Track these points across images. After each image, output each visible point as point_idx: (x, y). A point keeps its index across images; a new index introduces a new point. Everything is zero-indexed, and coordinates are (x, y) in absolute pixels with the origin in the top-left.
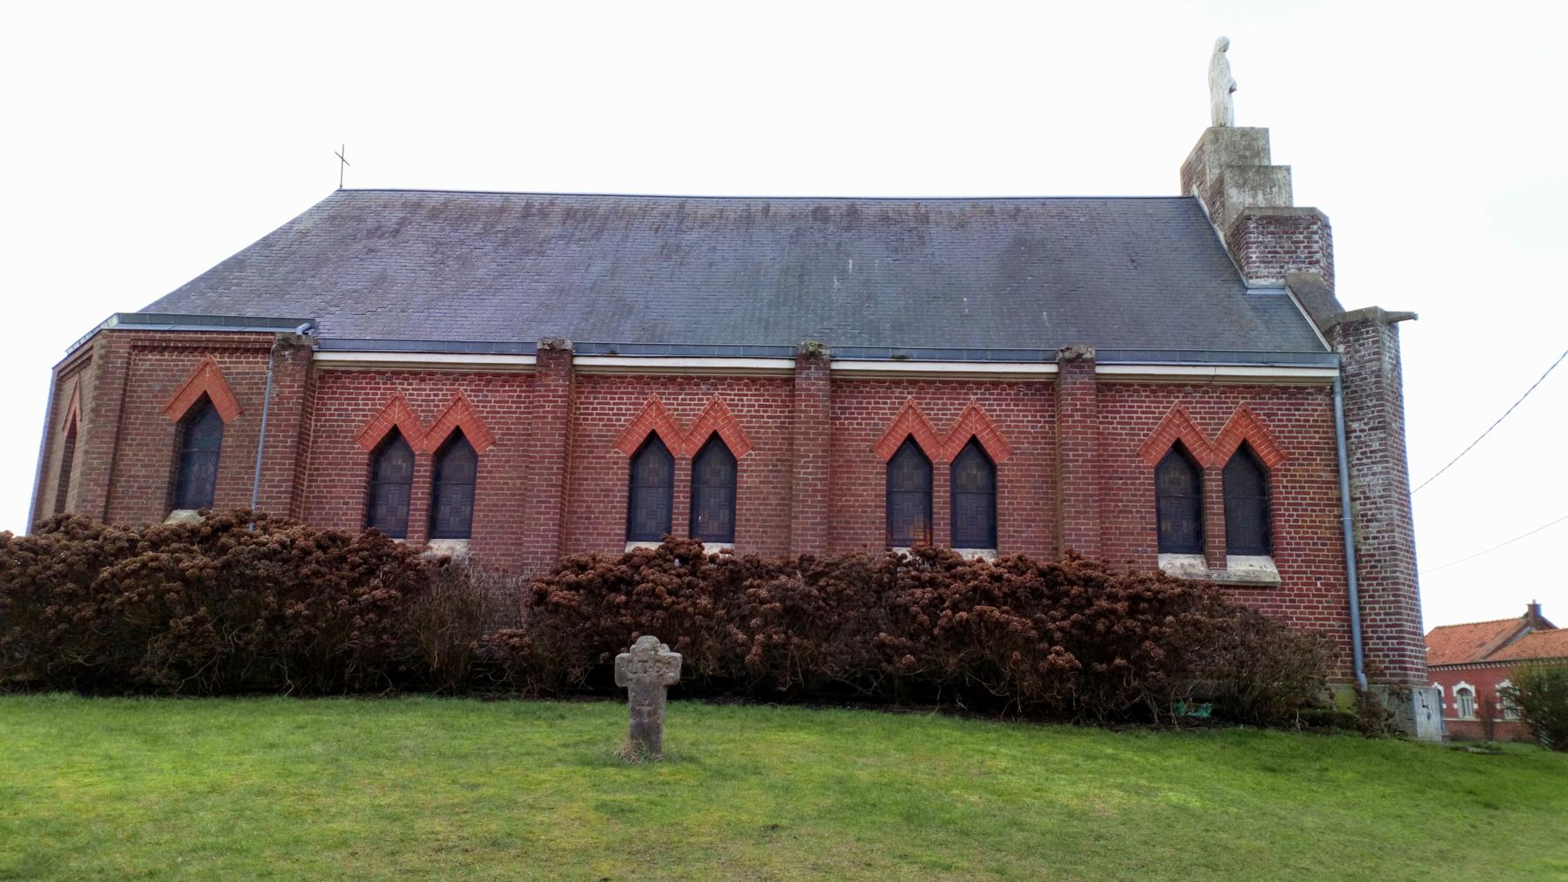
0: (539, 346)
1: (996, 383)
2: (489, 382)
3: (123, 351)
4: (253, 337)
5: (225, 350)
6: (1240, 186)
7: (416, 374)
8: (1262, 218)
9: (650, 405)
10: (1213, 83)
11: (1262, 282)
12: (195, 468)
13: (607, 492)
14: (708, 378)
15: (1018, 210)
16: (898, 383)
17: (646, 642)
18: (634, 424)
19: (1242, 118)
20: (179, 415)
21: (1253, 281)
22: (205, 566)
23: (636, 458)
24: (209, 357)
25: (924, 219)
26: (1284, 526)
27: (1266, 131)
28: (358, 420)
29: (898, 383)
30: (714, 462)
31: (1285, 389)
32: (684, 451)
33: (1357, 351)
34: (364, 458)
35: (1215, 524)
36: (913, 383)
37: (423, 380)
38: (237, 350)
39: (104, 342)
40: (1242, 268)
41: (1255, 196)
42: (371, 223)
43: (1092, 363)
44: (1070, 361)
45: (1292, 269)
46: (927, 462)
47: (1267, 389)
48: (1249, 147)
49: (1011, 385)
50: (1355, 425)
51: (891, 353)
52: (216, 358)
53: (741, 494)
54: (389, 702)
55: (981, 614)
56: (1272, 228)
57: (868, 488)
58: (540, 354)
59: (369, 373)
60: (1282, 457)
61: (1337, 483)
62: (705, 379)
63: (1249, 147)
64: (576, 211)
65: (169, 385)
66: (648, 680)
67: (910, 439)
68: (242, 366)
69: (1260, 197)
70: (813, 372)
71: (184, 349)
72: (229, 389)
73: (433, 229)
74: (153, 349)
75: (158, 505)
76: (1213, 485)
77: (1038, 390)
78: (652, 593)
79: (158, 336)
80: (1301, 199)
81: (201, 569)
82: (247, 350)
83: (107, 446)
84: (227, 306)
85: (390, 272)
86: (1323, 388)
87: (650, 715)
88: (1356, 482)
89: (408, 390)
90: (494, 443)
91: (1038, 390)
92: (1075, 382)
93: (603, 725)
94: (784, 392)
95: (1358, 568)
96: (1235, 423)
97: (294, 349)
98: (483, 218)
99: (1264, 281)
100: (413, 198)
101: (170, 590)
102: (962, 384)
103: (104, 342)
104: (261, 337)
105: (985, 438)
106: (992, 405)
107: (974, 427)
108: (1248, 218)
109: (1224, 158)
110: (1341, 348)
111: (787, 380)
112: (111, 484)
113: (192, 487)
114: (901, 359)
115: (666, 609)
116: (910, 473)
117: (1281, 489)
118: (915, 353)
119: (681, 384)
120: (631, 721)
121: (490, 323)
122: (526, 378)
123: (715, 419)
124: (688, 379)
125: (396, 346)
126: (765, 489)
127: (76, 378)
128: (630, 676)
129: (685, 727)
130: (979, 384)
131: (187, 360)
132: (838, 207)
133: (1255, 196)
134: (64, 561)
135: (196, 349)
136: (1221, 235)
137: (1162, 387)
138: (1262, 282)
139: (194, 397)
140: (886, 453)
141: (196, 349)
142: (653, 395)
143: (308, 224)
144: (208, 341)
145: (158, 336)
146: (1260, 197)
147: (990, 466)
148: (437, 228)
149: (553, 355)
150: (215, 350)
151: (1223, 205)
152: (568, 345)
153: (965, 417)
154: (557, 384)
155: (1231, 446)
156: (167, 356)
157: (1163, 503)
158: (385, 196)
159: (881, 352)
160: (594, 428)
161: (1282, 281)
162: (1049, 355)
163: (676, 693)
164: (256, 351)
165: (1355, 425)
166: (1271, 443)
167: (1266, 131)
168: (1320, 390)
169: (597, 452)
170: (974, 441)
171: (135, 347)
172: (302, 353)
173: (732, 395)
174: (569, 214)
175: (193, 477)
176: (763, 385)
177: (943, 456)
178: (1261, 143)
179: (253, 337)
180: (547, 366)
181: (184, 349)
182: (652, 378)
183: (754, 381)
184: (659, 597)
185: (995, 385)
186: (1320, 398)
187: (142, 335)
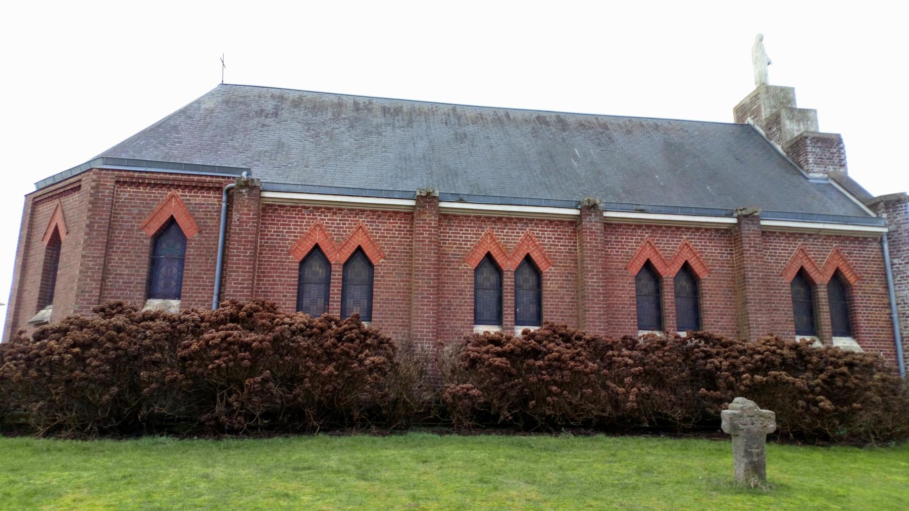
0: (418, 194)
1: (697, 229)
2: (379, 216)
3: (110, 184)
4: (208, 179)
5: (186, 187)
6: (791, 119)
7: (329, 209)
8: (813, 138)
9: (486, 235)
10: (756, 61)
11: (816, 175)
12: (163, 270)
13: (461, 292)
14: (522, 219)
15: (657, 125)
16: (639, 227)
17: (740, 402)
18: (476, 247)
19: (774, 80)
20: (153, 231)
21: (811, 175)
22: (263, 340)
23: (303, 263)
24: (173, 191)
25: (605, 126)
26: (862, 317)
27: (793, 89)
28: (294, 238)
29: (639, 227)
30: (358, 265)
31: (857, 238)
32: (337, 258)
33: (895, 218)
34: (296, 265)
35: (825, 317)
36: (649, 227)
37: (335, 213)
38: (195, 187)
39: (94, 177)
40: (802, 167)
41: (799, 126)
42: (254, 106)
43: (758, 219)
44: (746, 216)
45: (831, 169)
46: (328, 264)
47: (847, 238)
48: (785, 97)
49: (707, 230)
50: (896, 261)
51: (635, 207)
52: (179, 193)
53: (545, 294)
54: (379, 439)
55: (775, 377)
56: (819, 144)
57: (626, 291)
58: (419, 199)
59: (297, 207)
60: (858, 278)
61: (888, 294)
62: (520, 220)
63: (785, 97)
64: (389, 109)
65: (146, 211)
66: (755, 430)
67: (359, 249)
68: (199, 198)
69: (802, 126)
70: (593, 218)
71: (156, 185)
72: (191, 214)
73: (299, 114)
74: (131, 184)
75: (139, 295)
76: (823, 294)
77: (722, 233)
78: (558, 359)
79: (136, 175)
80: (825, 127)
81: (261, 342)
82: (202, 188)
83: (99, 252)
84: (178, 155)
85: (284, 140)
86: (878, 239)
87: (758, 455)
88: (899, 294)
89: (325, 219)
90: (385, 258)
91: (722, 233)
92: (748, 230)
93: (728, 462)
94: (570, 229)
95: (903, 345)
96: (832, 257)
97: (236, 190)
98: (330, 109)
99: (817, 175)
100: (278, 93)
101: (243, 359)
102: (678, 228)
103: (94, 177)
104: (214, 179)
105: (693, 263)
106: (698, 243)
107: (687, 256)
108: (806, 138)
109: (772, 103)
110: (885, 216)
111: (574, 222)
112: (103, 279)
113: (161, 284)
114: (642, 211)
115: (571, 370)
116: (489, 276)
117: (859, 297)
118: (650, 208)
119: (505, 222)
120: (746, 460)
121: (368, 177)
122: (409, 215)
123: (528, 245)
124: (510, 219)
125: (317, 190)
126: (562, 292)
127: (57, 202)
128: (742, 427)
129: (790, 466)
130: (688, 229)
131: (156, 192)
132: (551, 117)
133: (799, 126)
134: (150, 337)
135: (164, 185)
136: (779, 148)
137: (792, 234)
138: (816, 175)
139: (164, 219)
140: (474, 263)
141: (164, 185)
142: (487, 229)
143: (209, 105)
144: (174, 180)
145: (136, 175)
146: (802, 126)
147: (537, 273)
148: (302, 113)
149: (427, 200)
150: (179, 186)
151: (780, 129)
152: (437, 193)
153: (681, 249)
154: (431, 219)
155: (830, 272)
156: (141, 189)
157: (480, 293)
158: (256, 91)
159: (629, 207)
160: (451, 250)
161: (826, 175)
162: (728, 212)
163: (771, 438)
164: (209, 189)
165: (896, 261)
166: (852, 270)
167: (793, 89)
168: (875, 240)
169: (453, 265)
170: (489, 256)
171: (117, 182)
172: (254, 191)
173: (537, 231)
174: (385, 110)
175: (161, 276)
176: (557, 225)
177: (509, 265)
178: (791, 95)
179: (208, 179)
180: (424, 207)
181: (156, 185)
182: (487, 218)
183: (551, 222)
184: (564, 362)
185: (698, 229)
186: (875, 245)
187: (125, 174)
